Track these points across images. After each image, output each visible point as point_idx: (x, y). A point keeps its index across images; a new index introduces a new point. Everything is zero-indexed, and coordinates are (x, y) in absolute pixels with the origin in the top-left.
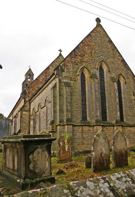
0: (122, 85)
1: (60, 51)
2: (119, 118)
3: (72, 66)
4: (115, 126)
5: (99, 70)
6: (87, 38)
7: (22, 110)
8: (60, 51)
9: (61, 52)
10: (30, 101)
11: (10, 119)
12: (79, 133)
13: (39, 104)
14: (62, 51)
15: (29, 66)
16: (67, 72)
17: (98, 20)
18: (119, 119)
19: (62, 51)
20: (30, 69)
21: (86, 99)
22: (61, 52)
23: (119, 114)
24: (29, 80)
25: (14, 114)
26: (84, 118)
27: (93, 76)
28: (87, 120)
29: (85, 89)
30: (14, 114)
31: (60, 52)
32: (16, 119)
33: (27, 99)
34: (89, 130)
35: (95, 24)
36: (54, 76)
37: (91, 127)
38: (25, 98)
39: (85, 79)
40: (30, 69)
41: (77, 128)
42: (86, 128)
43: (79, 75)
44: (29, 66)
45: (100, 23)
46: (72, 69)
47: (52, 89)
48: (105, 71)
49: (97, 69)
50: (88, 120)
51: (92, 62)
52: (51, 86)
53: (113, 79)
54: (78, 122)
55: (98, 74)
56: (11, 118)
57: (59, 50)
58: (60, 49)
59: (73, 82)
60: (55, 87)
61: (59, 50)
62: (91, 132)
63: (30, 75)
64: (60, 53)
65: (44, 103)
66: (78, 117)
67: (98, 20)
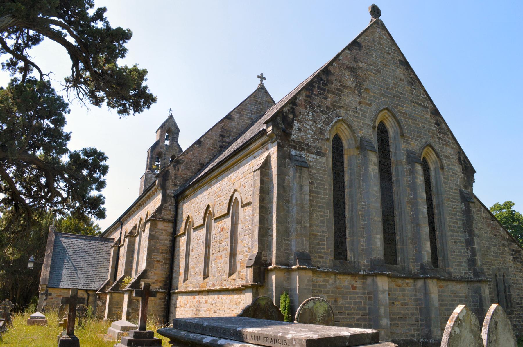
0: (432, 174)
1: (262, 78)
2: (427, 258)
3: (313, 116)
4: (421, 278)
5: (378, 132)
6: (349, 50)
7: (153, 220)
8: (262, 78)
9: (264, 82)
10: (180, 197)
11: (112, 237)
12: (328, 292)
13: (208, 206)
14: (265, 79)
15: (170, 110)
16: (300, 130)
17: (375, 11)
18: (430, 260)
19: (265, 79)
20: (171, 117)
21: (344, 203)
22: (264, 82)
23: (428, 246)
24: (167, 143)
25: (128, 227)
26: (340, 252)
27: (363, 146)
28: (346, 259)
29: (343, 176)
30: (128, 227)
31: (261, 81)
32: (132, 239)
33: (170, 191)
34: (354, 288)
35: (367, 20)
36: (265, 138)
37: (357, 278)
38: (163, 187)
39: (342, 150)
40: (171, 117)
41: (321, 279)
42: (345, 281)
43: (328, 140)
44: (170, 110)
45: (380, 18)
46: (311, 123)
47: (259, 172)
48: (391, 133)
49: (374, 127)
50: (349, 258)
51: (361, 110)
52: (260, 160)
53: (413, 158)
54: (325, 263)
55: (374, 140)
56: (116, 236)
57: (259, 77)
58: (262, 74)
59: (315, 157)
60: (267, 162)
61: (259, 77)
62: (357, 293)
63: (169, 131)
64: (260, 83)
65: (227, 205)
66: (324, 249)
67: (375, 11)
